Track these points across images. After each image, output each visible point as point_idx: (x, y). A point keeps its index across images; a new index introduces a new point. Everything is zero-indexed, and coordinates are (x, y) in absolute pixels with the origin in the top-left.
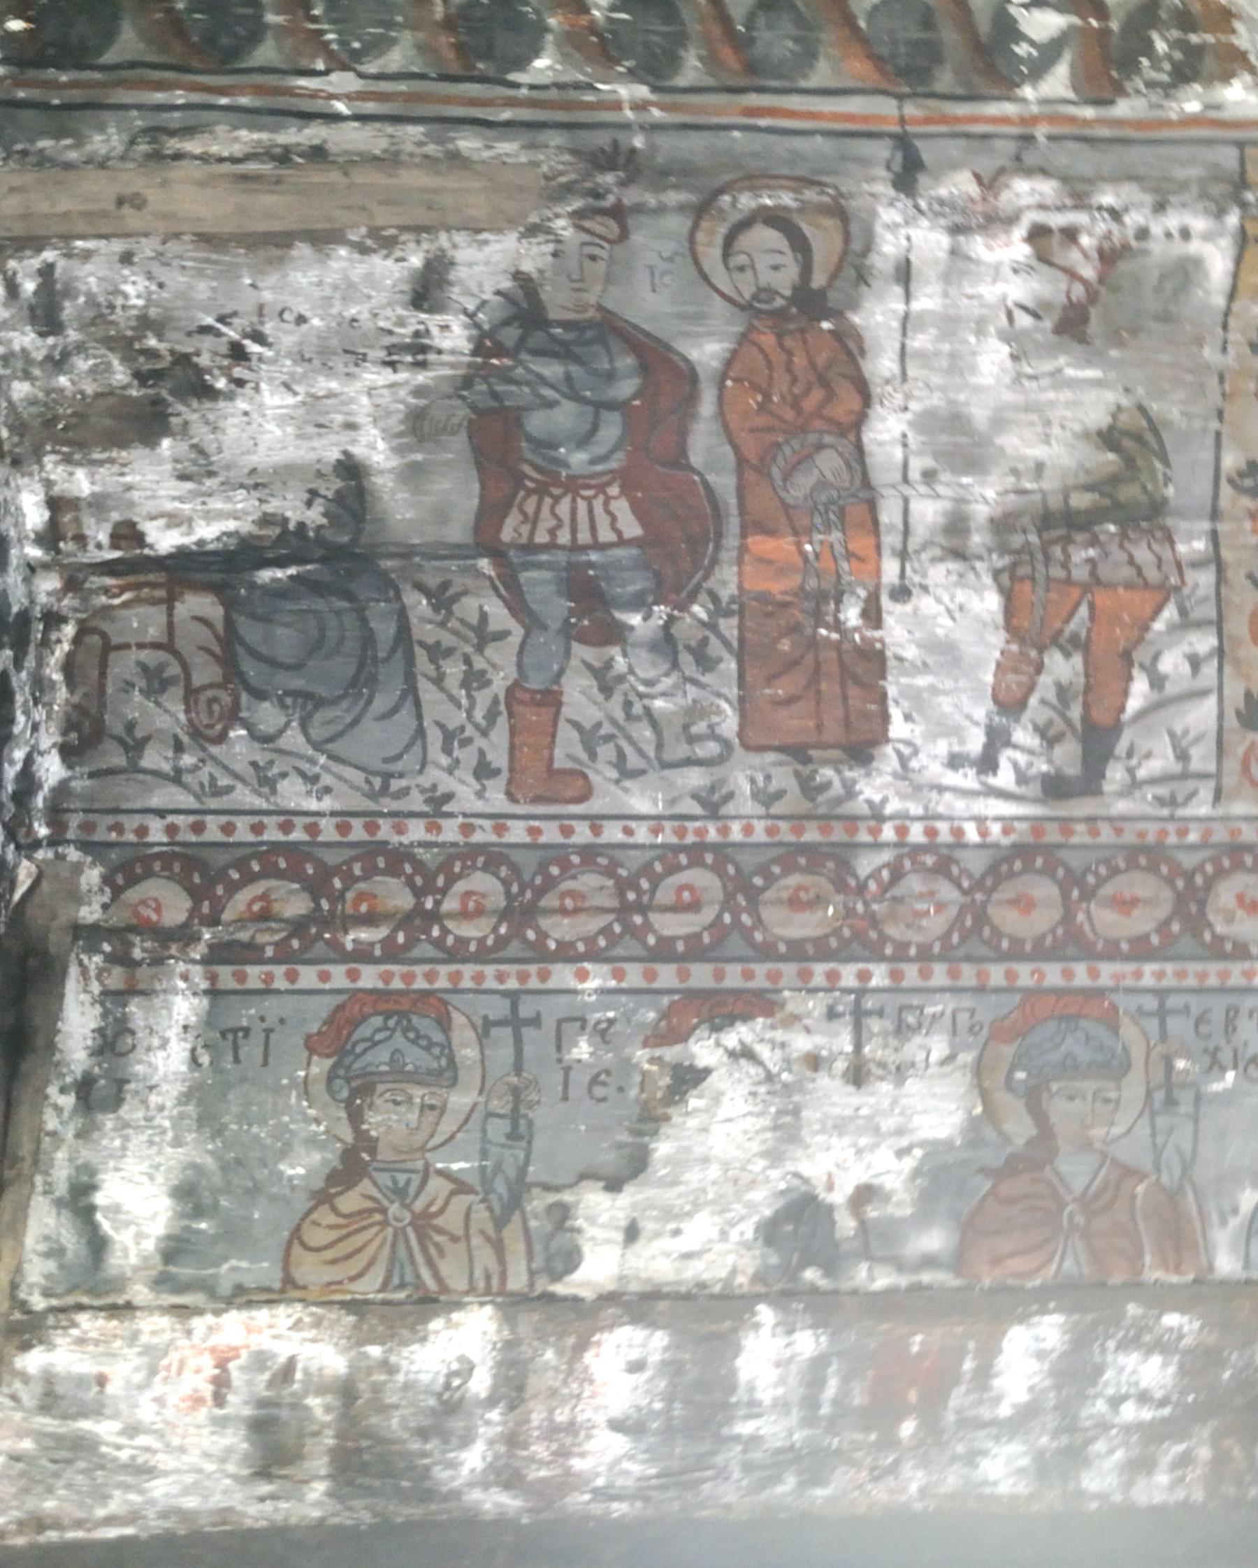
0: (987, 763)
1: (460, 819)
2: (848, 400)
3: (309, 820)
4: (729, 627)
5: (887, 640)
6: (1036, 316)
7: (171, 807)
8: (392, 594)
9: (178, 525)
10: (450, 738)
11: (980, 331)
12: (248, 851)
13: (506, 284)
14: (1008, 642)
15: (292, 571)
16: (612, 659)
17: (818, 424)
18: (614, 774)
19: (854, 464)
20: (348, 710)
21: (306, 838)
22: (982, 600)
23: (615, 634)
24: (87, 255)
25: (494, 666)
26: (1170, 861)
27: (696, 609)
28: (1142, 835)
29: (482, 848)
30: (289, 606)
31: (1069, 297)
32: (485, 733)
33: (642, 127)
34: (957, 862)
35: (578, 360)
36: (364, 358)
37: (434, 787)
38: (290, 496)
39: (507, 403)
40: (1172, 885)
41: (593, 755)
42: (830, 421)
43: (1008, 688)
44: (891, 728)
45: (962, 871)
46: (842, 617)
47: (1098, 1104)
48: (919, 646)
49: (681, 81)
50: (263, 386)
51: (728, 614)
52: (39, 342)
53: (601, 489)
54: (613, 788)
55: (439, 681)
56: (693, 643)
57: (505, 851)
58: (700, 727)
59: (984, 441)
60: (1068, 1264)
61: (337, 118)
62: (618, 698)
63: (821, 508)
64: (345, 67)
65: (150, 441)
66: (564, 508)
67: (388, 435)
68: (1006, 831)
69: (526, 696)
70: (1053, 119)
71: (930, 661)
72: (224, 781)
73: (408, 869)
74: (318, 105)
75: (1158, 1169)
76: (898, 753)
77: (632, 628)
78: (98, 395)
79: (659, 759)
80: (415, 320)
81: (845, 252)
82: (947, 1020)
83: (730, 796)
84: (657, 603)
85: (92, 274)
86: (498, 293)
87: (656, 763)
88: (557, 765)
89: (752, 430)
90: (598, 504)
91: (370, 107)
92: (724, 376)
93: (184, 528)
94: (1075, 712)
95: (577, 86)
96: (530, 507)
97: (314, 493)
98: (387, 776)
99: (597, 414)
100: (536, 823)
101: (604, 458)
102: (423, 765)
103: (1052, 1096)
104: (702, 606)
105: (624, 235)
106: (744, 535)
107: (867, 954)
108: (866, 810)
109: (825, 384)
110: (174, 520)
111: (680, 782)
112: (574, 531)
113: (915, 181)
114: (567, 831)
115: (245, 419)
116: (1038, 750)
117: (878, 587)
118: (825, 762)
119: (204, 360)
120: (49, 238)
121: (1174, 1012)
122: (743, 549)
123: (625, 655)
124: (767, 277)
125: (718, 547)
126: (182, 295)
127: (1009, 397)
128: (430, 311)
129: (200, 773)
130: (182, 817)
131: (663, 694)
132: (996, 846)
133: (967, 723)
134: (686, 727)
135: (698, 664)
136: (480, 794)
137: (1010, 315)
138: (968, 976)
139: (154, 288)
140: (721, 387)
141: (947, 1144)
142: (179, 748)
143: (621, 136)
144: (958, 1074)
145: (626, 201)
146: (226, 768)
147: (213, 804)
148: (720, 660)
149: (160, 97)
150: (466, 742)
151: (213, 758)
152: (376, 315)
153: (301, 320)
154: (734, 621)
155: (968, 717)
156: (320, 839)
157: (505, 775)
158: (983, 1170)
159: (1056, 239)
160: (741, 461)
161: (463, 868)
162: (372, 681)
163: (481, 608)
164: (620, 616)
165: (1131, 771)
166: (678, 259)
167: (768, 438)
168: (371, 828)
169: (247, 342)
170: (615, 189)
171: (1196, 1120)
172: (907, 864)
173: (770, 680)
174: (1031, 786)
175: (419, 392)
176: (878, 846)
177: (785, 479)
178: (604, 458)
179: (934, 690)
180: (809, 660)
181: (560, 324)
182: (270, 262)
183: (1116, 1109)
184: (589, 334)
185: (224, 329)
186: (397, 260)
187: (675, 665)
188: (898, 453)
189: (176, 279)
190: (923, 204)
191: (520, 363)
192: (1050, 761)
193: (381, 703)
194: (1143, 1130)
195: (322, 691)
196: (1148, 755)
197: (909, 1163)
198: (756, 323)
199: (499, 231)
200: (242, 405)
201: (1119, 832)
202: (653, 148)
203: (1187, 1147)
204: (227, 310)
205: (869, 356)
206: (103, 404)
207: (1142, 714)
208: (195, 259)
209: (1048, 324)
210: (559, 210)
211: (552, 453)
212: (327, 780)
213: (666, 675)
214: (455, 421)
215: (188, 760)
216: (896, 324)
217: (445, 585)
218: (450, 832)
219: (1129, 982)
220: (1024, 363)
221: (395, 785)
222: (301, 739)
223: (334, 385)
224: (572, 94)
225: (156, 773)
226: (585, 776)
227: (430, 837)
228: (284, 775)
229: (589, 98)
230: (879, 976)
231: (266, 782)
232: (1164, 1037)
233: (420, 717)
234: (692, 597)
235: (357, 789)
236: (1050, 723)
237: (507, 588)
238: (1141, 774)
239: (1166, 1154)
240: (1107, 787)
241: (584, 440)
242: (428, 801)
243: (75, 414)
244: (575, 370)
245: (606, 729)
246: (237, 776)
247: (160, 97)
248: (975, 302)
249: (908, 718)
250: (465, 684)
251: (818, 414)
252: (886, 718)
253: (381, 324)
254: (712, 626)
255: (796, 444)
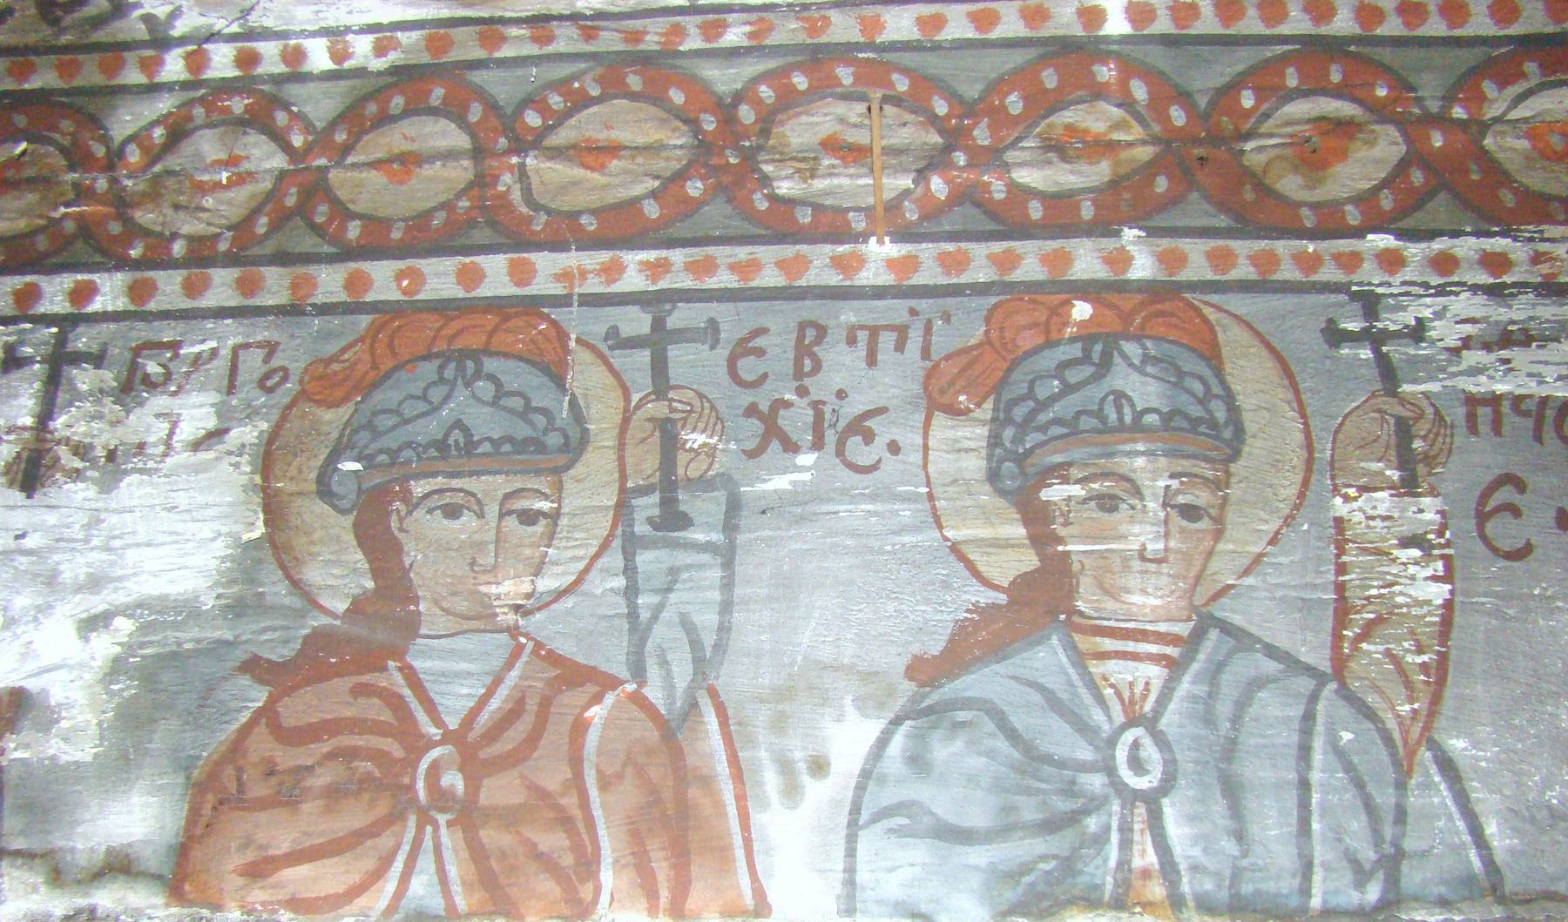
26: (692, 84)
34: (286, 106)
40: (693, 123)
45: (295, 117)
47: (511, 522)
60: (422, 887)
68: (380, 50)
75: (639, 673)
82: (221, 365)
103: (412, 507)
107: (98, 258)
108: (141, 32)
121: (683, 335)
132: (361, 72)
138: (276, 285)
141: (188, 610)
144: (225, 467)
158: (254, 667)
171: (727, 555)
172: (199, 112)
176: (154, 89)
183: (550, 537)
194: (607, 583)
197: (104, 646)
203: (707, 620)
219: (594, 286)
230: (110, 291)
232: (661, 382)
239: (659, 633)
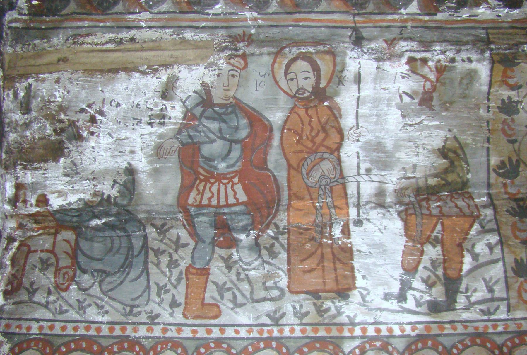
0: (402, 297)
1: (162, 326)
2: (334, 137)
3: (97, 325)
4: (283, 239)
5: (353, 243)
6: (412, 98)
7: (42, 318)
8: (142, 228)
9: (62, 196)
10: (161, 289)
11: (389, 105)
12: (71, 339)
13: (199, 88)
14: (407, 242)
15: (104, 221)
16: (232, 254)
17: (322, 149)
18: (231, 305)
19: (336, 167)
20: (119, 277)
21: (96, 334)
22: (394, 224)
23: (233, 243)
24: (44, 80)
25: (181, 258)
27: (269, 231)
28: (476, 328)
29: (170, 339)
30: (101, 234)
31: (424, 89)
32: (175, 287)
33: (254, 26)
35: (225, 121)
36: (140, 121)
37: (152, 311)
38: (106, 183)
39: (195, 141)
41: (222, 297)
42: (328, 148)
43: (409, 263)
44: (356, 282)
46: (333, 233)
48: (368, 245)
49: (270, 11)
50: (101, 135)
51: (283, 233)
52: (22, 117)
53: (231, 179)
54: (231, 312)
55: (157, 265)
56: (268, 246)
57: (181, 341)
58: (270, 284)
59: (392, 156)
61: (142, 28)
62: (234, 271)
63: (323, 187)
64: (146, 11)
65: (56, 159)
66: (215, 188)
67: (147, 156)
69: (194, 271)
70: (413, 20)
71: (372, 251)
72: (65, 308)
73: (137, 349)
74: (135, 24)
76: (360, 293)
77: (241, 240)
78: (41, 139)
79: (252, 298)
80: (161, 103)
81: (334, 71)
83: (283, 315)
84: (252, 230)
85: (44, 88)
86: (195, 92)
87: (250, 300)
88: (206, 301)
89: (295, 152)
90: (229, 186)
91: (153, 24)
92: (283, 128)
93: (64, 198)
94: (440, 272)
95: (231, 14)
96: (201, 187)
97: (115, 182)
98: (132, 307)
99: (231, 145)
100: (196, 328)
101: (233, 165)
102: (148, 300)
104: (271, 230)
105: (246, 65)
106: (290, 199)
109: (324, 130)
110: (61, 194)
111: (261, 309)
112: (218, 199)
113: (361, 43)
114: (209, 332)
115: (92, 150)
116: (425, 290)
117: (348, 220)
118: (327, 299)
119: (80, 124)
120: (31, 74)
122: (289, 206)
123: (238, 252)
124: (302, 83)
125: (278, 205)
126: (76, 96)
127: (402, 135)
128: (168, 100)
129: (56, 304)
130: (46, 323)
131: (254, 269)
133: (391, 279)
134: (264, 283)
135: (270, 255)
136: (171, 315)
137: (401, 96)
139: (66, 93)
140: (282, 132)
142: (49, 293)
143: (246, 30)
145: (247, 52)
146: (66, 301)
147: (59, 317)
148: (280, 253)
149: (80, 24)
150: (168, 291)
151: (62, 297)
152: (147, 102)
153: (118, 105)
154: (286, 236)
155: (391, 276)
156: (101, 334)
157: (183, 306)
159: (419, 63)
160: (290, 166)
161: (162, 348)
162: (131, 265)
163: (178, 234)
164: (236, 235)
165: (468, 298)
166: (267, 76)
167: (301, 155)
168: (123, 330)
169: (97, 115)
170: (243, 48)
173: (302, 261)
174: (423, 307)
175: (160, 136)
177: (308, 174)
178: (233, 165)
179: (375, 264)
180: (319, 251)
181: (219, 105)
182: (109, 80)
184: (230, 110)
185: (89, 110)
186: (157, 78)
187: (260, 256)
188: (355, 161)
189: (74, 89)
190: (365, 50)
191: (201, 123)
192: (430, 295)
193: (133, 274)
195: (109, 269)
196: (475, 290)
198: (297, 103)
199: (197, 65)
200: (92, 143)
201: (466, 327)
202: (258, 34)
204: (91, 102)
205: (343, 117)
206: (41, 143)
207: (470, 271)
208: (82, 81)
209: (416, 101)
210: (221, 55)
211: (211, 163)
212: (107, 308)
213: (256, 260)
214: (174, 149)
215: (52, 298)
216: (354, 102)
217: (164, 225)
218: (157, 332)
220: (407, 119)
221: (136, 310)
222: (98, 290)
223: (128, 134)
224: (228, 17)
225: (39, 303)
226: (218, 306)
227: (149, 334)
228: (90, 305)
229: (235, 17)
231: (82, 308)
233: (148, 280)
234: (268, 226)
235: (119, 312)
236: (429, 277)
237: (189, 225)
238: (473, 299)
240: (458, 306)
241: (224, 158)
242: (148, 317)
243: (29, 148)
244: (223, 125)
245: (229, 285)
246: (70, 306)
247: (80, 24)
248: (387, 91)
249: (364, 277)
250: (169, 266)
251: (321, 144)
252: (354, 278)
253: (148, 106)
254: (276, 239)
255: (312, 158)
